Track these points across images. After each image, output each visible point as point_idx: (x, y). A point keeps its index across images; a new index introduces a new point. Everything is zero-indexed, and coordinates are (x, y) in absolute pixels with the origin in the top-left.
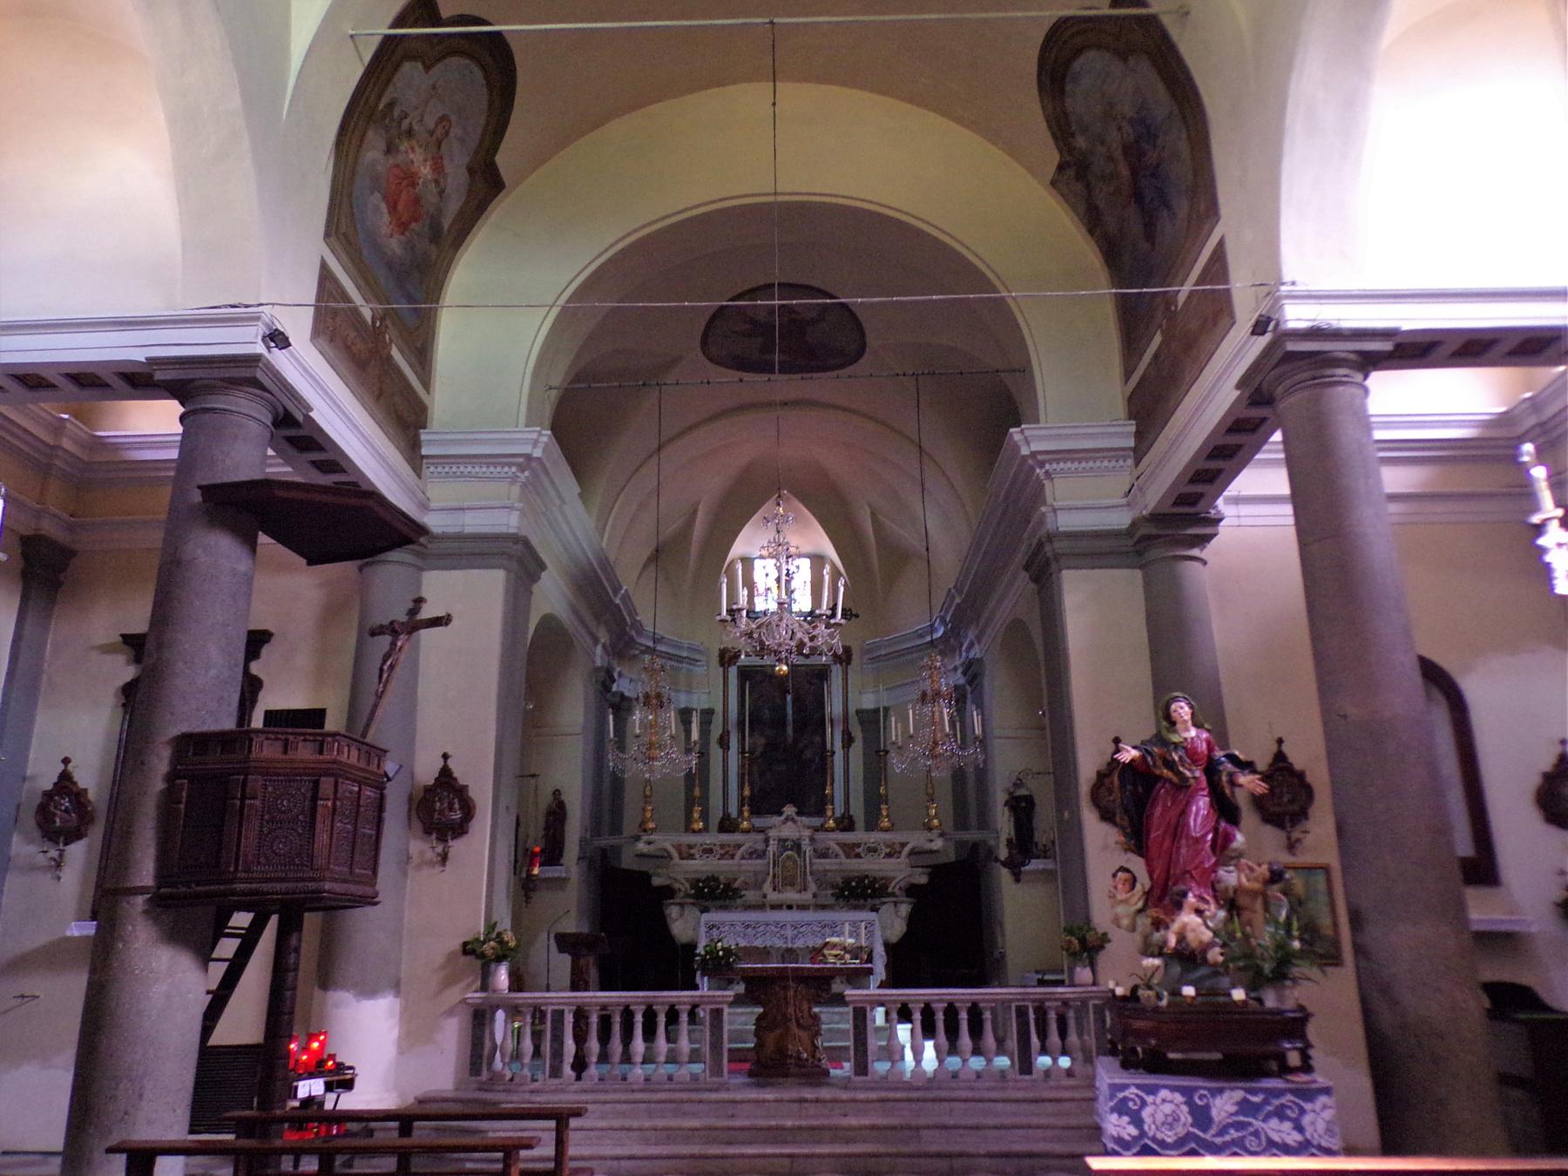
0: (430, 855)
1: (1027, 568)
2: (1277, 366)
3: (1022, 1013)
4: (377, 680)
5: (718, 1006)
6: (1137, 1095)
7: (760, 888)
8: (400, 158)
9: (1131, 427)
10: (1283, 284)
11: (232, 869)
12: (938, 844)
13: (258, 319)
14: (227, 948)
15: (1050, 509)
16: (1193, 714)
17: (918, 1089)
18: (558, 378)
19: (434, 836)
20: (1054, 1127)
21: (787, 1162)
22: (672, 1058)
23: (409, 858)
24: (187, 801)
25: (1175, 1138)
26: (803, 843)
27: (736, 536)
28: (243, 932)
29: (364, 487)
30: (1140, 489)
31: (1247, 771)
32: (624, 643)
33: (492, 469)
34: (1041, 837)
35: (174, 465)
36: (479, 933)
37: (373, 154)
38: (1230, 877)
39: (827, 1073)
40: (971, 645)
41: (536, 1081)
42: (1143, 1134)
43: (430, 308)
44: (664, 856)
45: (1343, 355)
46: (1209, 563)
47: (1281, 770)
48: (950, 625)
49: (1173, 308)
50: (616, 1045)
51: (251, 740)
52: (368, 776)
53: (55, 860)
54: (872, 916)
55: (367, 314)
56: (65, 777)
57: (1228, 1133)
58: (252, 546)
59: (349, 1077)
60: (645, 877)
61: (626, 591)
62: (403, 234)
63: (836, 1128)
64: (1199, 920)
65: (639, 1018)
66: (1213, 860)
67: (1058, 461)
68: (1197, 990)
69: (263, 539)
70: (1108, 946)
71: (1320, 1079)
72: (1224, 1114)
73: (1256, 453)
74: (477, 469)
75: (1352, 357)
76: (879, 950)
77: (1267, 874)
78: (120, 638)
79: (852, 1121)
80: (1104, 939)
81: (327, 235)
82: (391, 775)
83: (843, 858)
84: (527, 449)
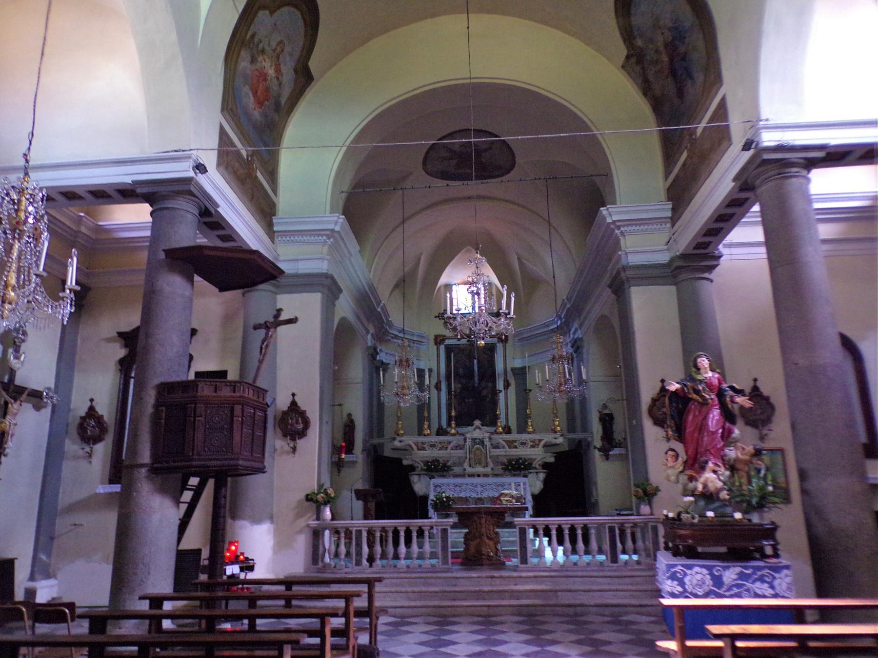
0: (287, 448)
1: (610, 286)
2: (756, 168)
3: (612, 530)
4: (259, 354)
5: (445, 527)
6: (682, 570)
7: (462, 466)
8: (258, 65)
9: (670, 205)
10: (761, 120)
11: (191, 454)
12: (560, 440)
13: (189, 157)
14: (187, 496)
15: (624, 253)
16: (710, 364)
17: (555, 571)
18: (346, 186)
19: (289, 437)
20: (631, 591)
21: (485, 609)
22: (421, 557)
23: (275, 450)
24: (166, 418)
25: (703, 593)
26: (485, 440)
27: (441, 275)
28: (194, 488)
29: (244, 247)
30: (675, 241)
31: (740, 395)
32: (383, 333)
33: (312, 238)
34: (618, 436)
35: (148, 239)
36: (314, 490)
37: (244, 64)
38: (731, 453)
39: (504, 564)
40: (576, 330)
41: (348, 568)
42: (685, 590)
43: (276, 150)
44: (407, 449)
45: (795, 160)
46: (714, 281)
47: (755, 393)
48: (563, 320)
49: (694, 137)
50: (390, 549)
51: (197, 385)
52: (258, 404)
53: (88, 453)
54: (525, 479)
55: (244, 153)
56: (92, 409)
57: (732, 590)
58: (191, 281)
59: (251, 564)
60: (399, 460)
61: (384, 304)
62: (261, 108)
63: (512, 591)
64: (715, 476)
65: (402, 534)
66: (722, 443)
67: (628, 225)
68: (715, 513)
69: (197, 278)
70: (659, 494)
71: (783, 561)
72: (730, 580)
73: (741, 219)
74: (305, 238)
75: (802, 161)
76: (529, 498)
77: (753, 451)
78: (116, 334)
79: (520, 587)
80: (657, 490)
81: (223, 110)
82: (269, 404)
83: (508, 449)
84: (331, 226)
